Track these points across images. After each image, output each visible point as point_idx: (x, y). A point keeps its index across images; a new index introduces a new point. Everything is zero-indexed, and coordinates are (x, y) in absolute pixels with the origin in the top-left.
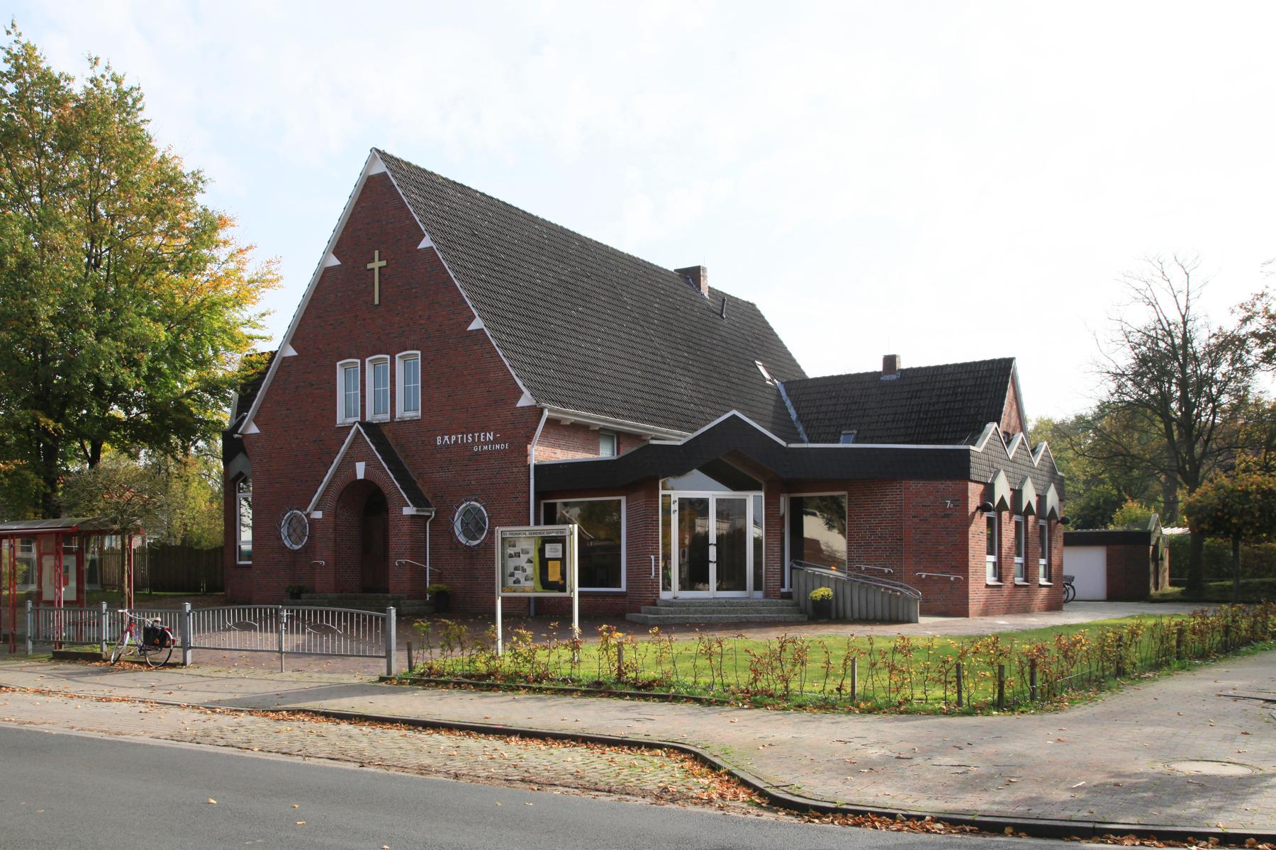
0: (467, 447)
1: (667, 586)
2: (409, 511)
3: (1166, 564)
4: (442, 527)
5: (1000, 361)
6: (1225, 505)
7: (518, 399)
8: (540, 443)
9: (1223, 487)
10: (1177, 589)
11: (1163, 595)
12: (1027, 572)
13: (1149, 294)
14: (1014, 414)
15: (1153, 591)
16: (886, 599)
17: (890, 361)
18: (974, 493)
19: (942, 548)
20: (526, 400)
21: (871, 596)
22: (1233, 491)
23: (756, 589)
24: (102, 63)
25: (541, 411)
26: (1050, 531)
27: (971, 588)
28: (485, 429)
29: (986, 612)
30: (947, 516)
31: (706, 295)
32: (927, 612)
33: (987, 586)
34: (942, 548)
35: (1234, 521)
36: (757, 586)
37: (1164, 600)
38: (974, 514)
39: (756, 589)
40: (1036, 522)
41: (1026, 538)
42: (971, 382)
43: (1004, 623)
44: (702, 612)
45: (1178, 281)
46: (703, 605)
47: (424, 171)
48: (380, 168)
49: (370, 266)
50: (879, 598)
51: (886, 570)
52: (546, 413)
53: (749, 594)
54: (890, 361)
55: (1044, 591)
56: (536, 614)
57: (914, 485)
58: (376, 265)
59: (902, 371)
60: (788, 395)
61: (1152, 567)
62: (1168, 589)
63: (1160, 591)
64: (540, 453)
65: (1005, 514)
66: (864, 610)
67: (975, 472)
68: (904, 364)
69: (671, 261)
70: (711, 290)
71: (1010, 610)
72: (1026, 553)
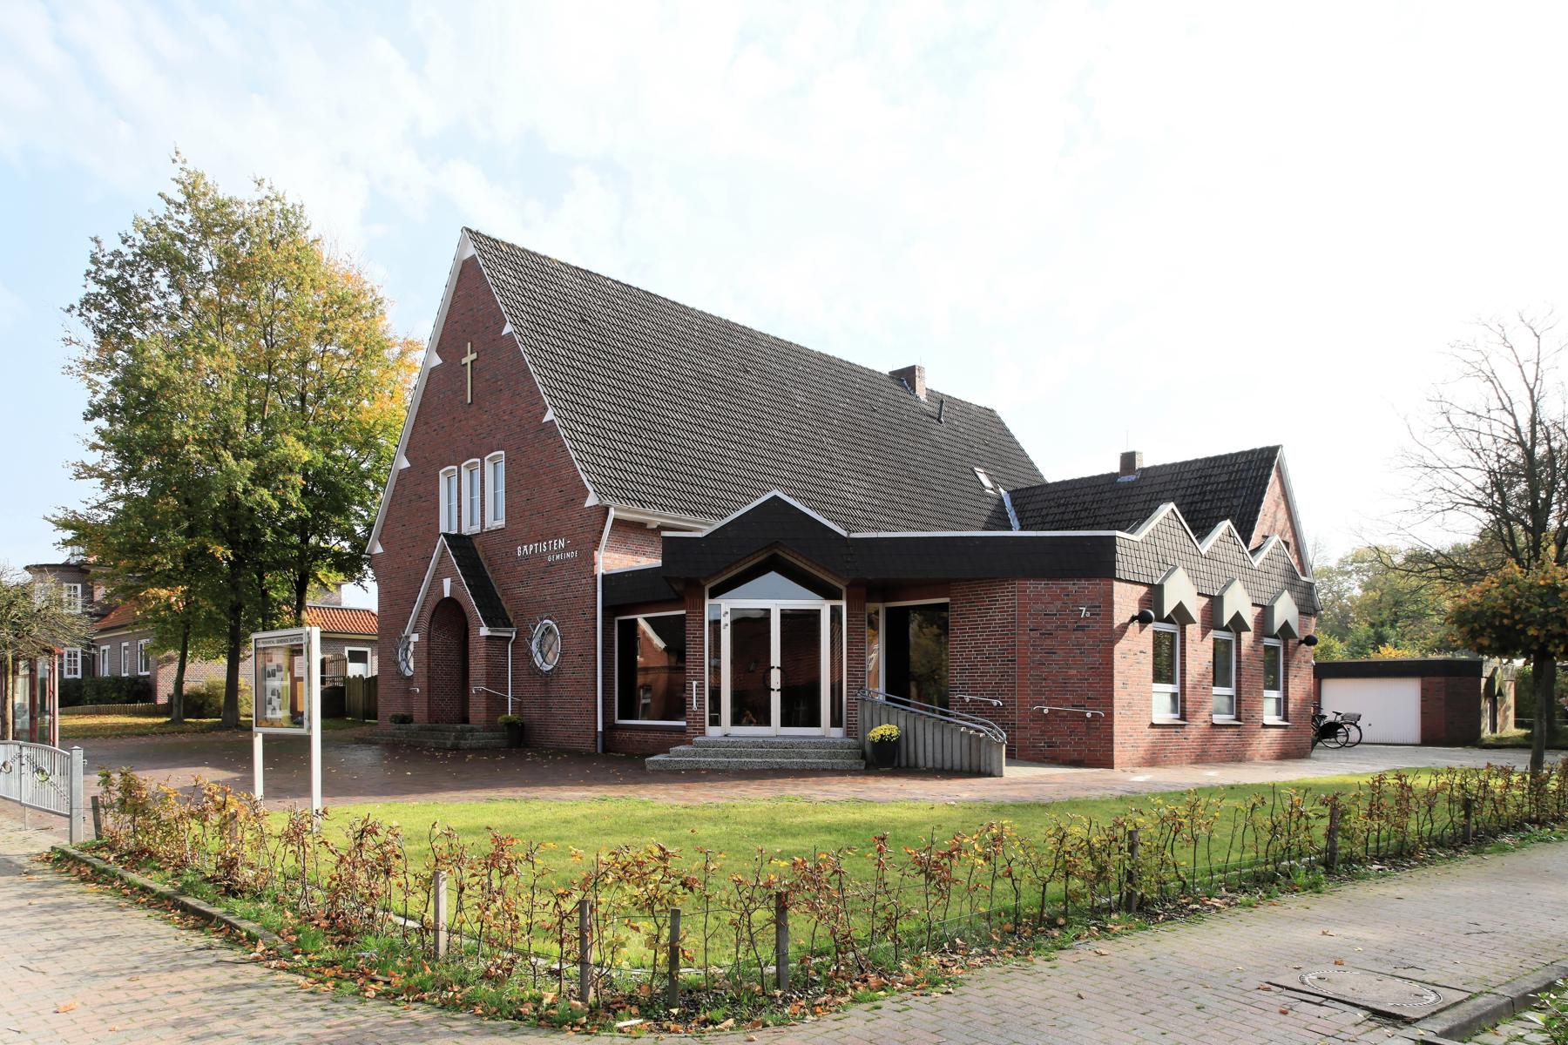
0: (542, 556)
1: (715, 721)
2: (484, 631)
3: (1510, 700)
4: (521, 646)
5: (1262, 450)
6: (1515, 609)
7: (586, 497)
8: (609, 548)
9: (1514, 581)
10: (1524, 731)
11: (1501, 739)
12: (1241, 707)
13: (1485, 367)
14: (1282, 515)
15: (1486, 733)
16: (965, 741)
17: (1128, 459)
18: (1126, 601)
19: (1073, 672)
20: (592, 501)
21: (947, 736)
22: (1531, 586)
23: (833, 725)
24: (266, 184)
25: (607, 509)
26: (1286, 653)
27: (1116, 728)
28: (557, 536)
29: (1153, 759)
30: (1081, 628)
31: (923, 397)
32: (1015, 756)
33: (1153, 725)
34: (1073, 672)
35: (1532, 632)
36: (836, 722)
37: (1500, 745)
38: (1124, 627)
39: (833, 725)
40: (1258, 639)
41: (1239, 662)
42: (1224, 478)
43: (1144, 777)
44: (725, 755)
45: (1526, 348)
46: (818, 744)
47: (534, 254)
48: (471, 251)
49: (464, 361)
50: (956, 741)
51: (995, 702)
52: (612, 513)
53: (826, 730)
54: (1128, 459)
55: (1273, 732)
56: (605, 750)
57: (1032, 587)
58: (467, 360)
59: (1143, 470)
60: (1013, 505)
61: (1486, 705)
62: (1510, 730)
63: (1498, 734)
64: (611, 560)
65: (1193, 631)
66: (938, 756)
67: (1123, 567)
68: (1146, 461)
69: (885, 363)
70: (931, 393)
71: (1201, 758)
72: (1238, 682)
